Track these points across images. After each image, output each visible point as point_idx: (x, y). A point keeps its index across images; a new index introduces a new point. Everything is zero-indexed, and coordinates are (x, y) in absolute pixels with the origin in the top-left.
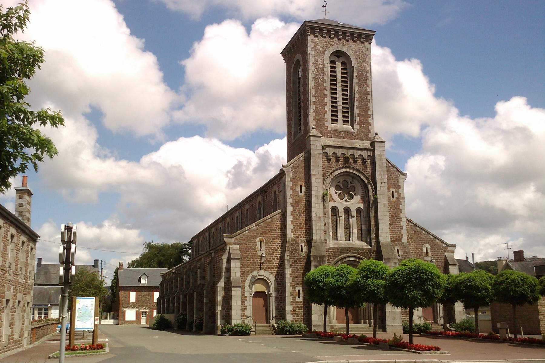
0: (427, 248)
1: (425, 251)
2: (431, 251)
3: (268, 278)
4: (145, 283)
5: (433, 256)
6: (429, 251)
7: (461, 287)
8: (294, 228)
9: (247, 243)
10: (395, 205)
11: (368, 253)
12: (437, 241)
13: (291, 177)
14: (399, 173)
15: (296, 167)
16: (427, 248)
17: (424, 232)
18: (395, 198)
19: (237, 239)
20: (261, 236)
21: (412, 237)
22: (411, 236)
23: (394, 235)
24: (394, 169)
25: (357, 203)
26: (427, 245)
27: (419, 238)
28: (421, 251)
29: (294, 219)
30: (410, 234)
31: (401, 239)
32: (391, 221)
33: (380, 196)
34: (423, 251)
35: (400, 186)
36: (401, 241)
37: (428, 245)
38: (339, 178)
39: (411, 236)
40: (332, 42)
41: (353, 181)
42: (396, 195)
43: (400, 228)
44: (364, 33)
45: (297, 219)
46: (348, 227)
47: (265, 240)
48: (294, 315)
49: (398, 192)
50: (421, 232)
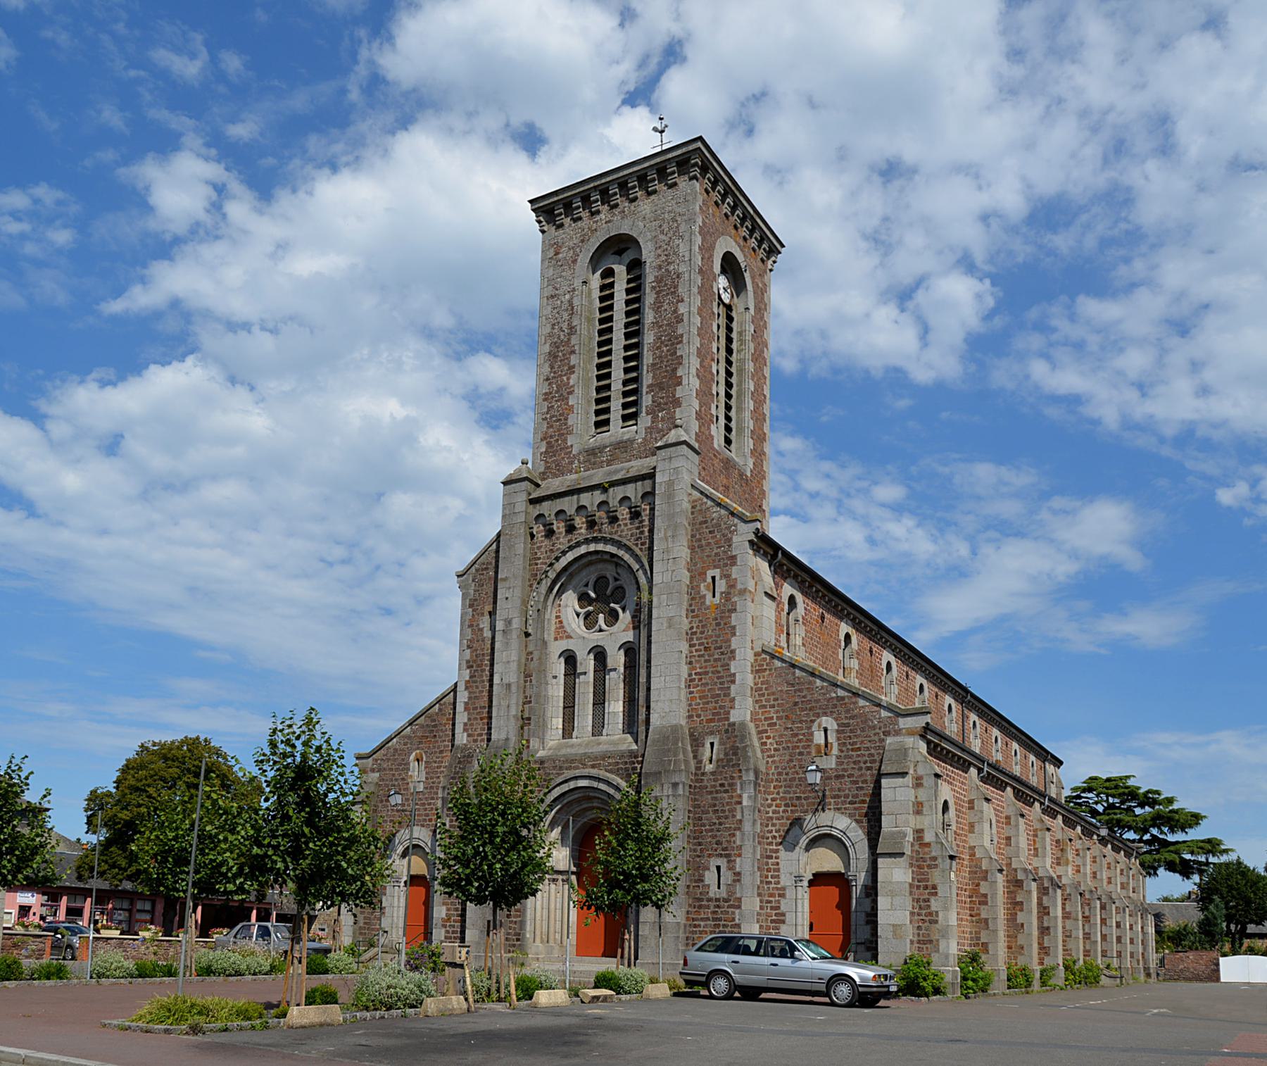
0: (826, 730)
1: (819, 738)
2: (838, 739)
3: (831, 827)
4: (413, 857)
5: (845, 753)
6: (832, 738)
7: (279, 868)
8: (469, 719)
9: (393, 767)
10: (718, 616)
11: (626, 763)
12: (862, 702)
13: (472, 597)
14: (736, 520)
15: (483, 570)
16: (826, 730)
17: (818, 682)
18: (717, 595)
19: (376, 760)
20: (418, 749)
21: (780, 702)
22: (776, 700)
23: (707, 703)
24: (723, 512)
25: (622, 629)
26: (829, 722)
27: (802, 702)
28: (808, 740)
29: (470, 698)
30: (773, 694)
31: (728, 713)
32: (704, 664)
33: (659, 599)
34: (812, 741)
35: (734, 558)
36: (728, 719)
37: (830, 719)
38: (584, 573)
39: (776, 700)
40: (597, 222)
41: (618, 573)
42: (721, 586)
43: (728, 682)
44: (669, 159)
45: (476, 697)
46: (600, 701)
47: (426, 755)
48: (448, 929)
49: (727, 576)
50: (810, 683)
